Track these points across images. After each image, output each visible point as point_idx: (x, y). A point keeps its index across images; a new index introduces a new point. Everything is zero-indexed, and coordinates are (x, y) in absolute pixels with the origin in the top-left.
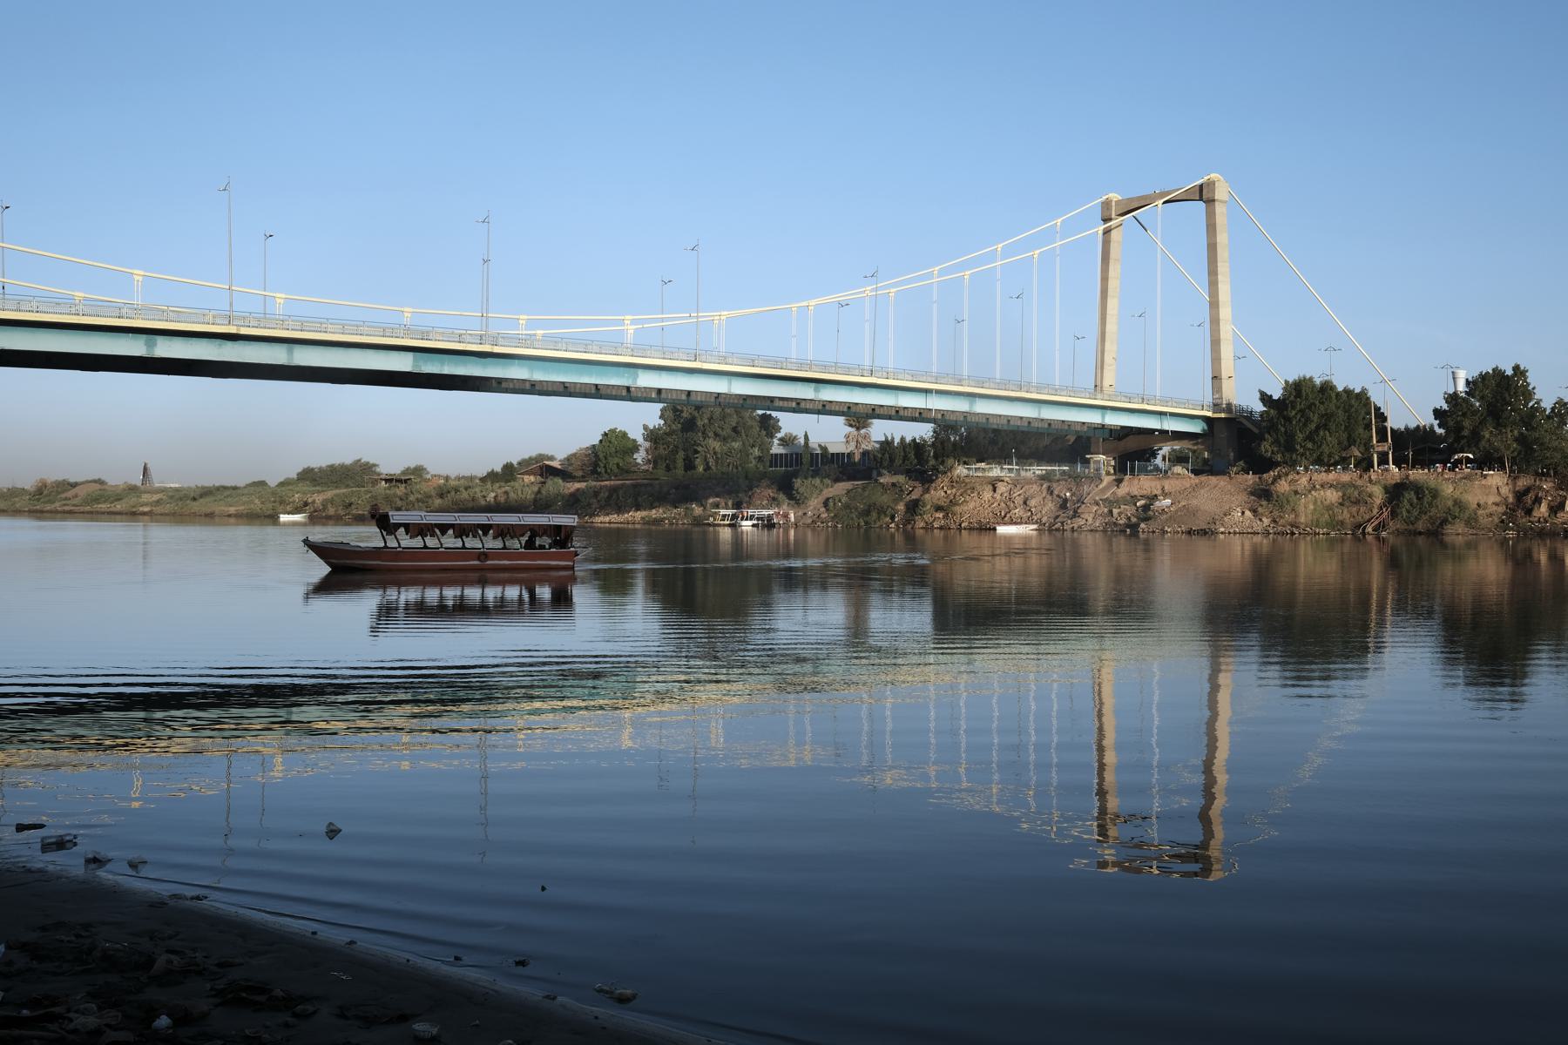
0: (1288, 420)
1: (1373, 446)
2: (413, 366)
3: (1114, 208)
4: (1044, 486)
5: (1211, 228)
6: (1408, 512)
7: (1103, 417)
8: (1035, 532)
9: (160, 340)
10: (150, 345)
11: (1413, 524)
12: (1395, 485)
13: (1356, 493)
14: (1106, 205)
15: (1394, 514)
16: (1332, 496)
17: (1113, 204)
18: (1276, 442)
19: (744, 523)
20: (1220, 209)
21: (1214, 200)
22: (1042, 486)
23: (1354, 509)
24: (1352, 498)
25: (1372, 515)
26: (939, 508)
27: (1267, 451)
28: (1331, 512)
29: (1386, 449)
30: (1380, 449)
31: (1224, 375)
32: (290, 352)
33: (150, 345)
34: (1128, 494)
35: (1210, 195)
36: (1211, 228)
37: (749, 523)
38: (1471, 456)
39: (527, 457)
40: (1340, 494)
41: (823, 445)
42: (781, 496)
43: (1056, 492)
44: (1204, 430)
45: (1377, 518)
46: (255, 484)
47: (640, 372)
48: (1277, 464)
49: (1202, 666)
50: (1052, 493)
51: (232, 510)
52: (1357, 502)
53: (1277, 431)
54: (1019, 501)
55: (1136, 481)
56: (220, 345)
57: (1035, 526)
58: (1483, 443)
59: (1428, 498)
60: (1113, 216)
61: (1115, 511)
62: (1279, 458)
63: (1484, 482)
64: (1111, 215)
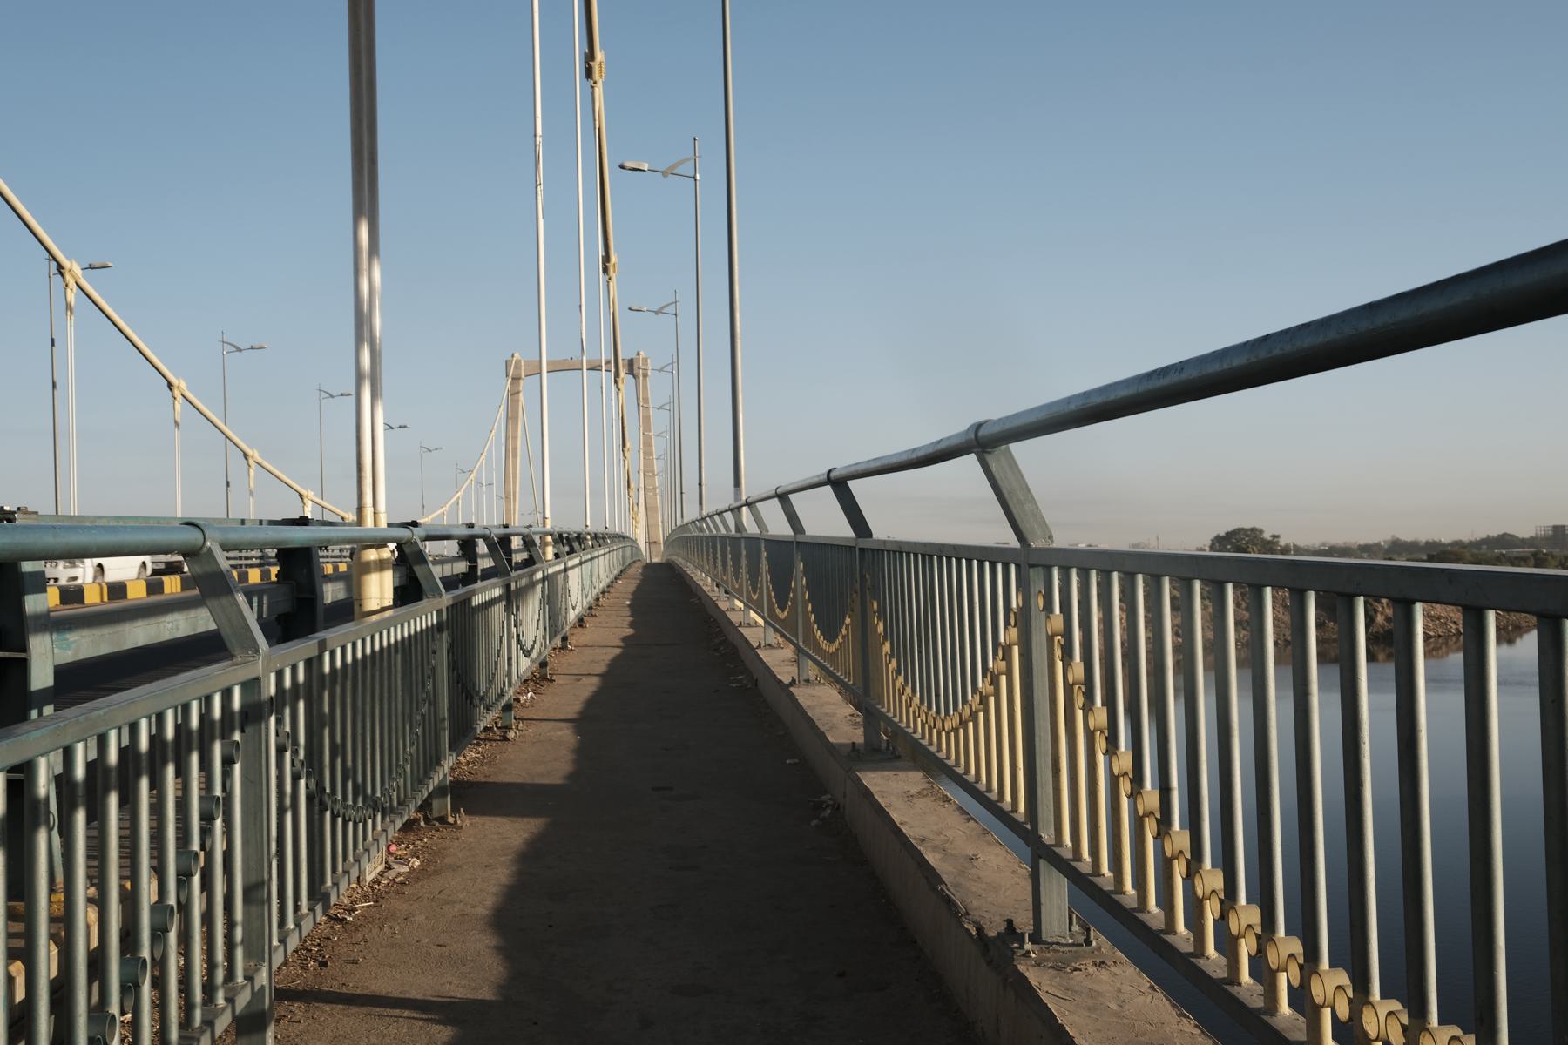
3: (523, 368)
60: (523, 376)
64: (521, 375)
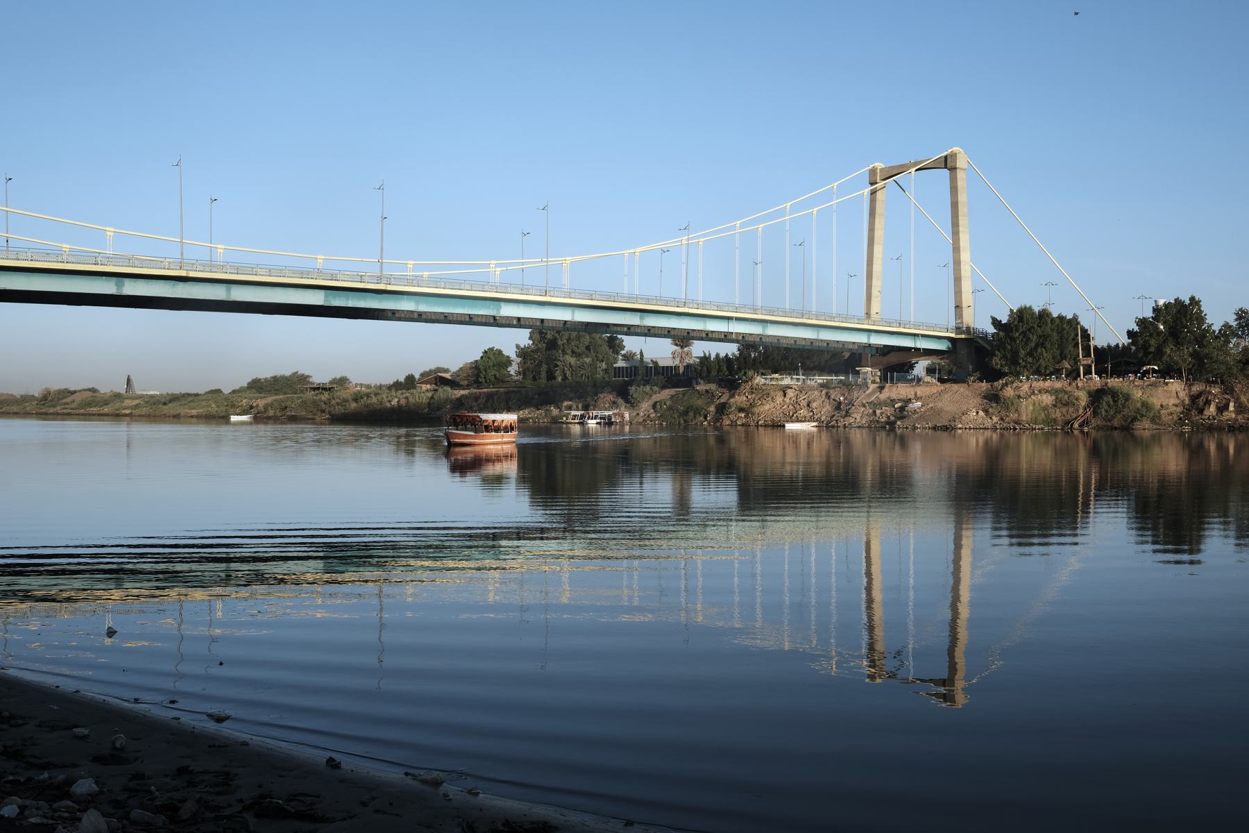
0: (1014, 340)
1: (1079, 360)
2: (325, 301)
3: (878, 175)
4: (824, 392)
5: (954, 189)
6: (1106, 411)
7: (869, 338)
8: (815, 429)
9: (127, 281)
10: (119, 286)
11: (1110, 421)
12: (1097, 390)
13: (1066, 397)
14: (873, 172)
15: (1095, 413)
16: (1048, 399)
17: (878, 171)
18: (1004, 357)
19: (590, 421)
20: (960, 175)
21: (956, 168)
22: (822, 392)
23: (1064, 410)
24: (1063, 400)
25: (1079, 414)
26: (741, 410)
27: (997, 364)
28: (1046, 412)
29: (1090, 362)
30: (1085, 362)
31: (965, 305)
32: (229, 290)
33: (119, 286)
34: (888, 398)
35: (953, 164)
36: (954, 189)
37: (594, 421)
38: (1156, 368)
39: (427, 370)
40: (1054, 397)
41: (654, 360)
42: (620, 401)
43: (832, 397)
44: (948, 348)
45: (1082, 416)
46: (212, 392)
47: (503, 304)
48: (1005, 375)
49: (952, 526)
50: (829, 398)
51: (194, 412)
52: (1067, 404)
53: (1005, 348)
54: (804, 403)
55: (895, 389)
56: (174, 285)
57: (815, 424)
58: (1165, 358)
59: (1121, 401)
61: (878, 412)
62: (1006, 369)
63: (1166, 388)
